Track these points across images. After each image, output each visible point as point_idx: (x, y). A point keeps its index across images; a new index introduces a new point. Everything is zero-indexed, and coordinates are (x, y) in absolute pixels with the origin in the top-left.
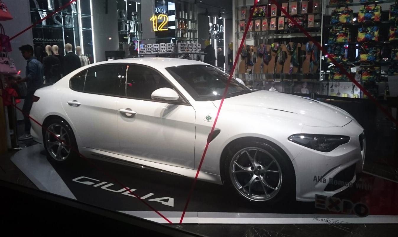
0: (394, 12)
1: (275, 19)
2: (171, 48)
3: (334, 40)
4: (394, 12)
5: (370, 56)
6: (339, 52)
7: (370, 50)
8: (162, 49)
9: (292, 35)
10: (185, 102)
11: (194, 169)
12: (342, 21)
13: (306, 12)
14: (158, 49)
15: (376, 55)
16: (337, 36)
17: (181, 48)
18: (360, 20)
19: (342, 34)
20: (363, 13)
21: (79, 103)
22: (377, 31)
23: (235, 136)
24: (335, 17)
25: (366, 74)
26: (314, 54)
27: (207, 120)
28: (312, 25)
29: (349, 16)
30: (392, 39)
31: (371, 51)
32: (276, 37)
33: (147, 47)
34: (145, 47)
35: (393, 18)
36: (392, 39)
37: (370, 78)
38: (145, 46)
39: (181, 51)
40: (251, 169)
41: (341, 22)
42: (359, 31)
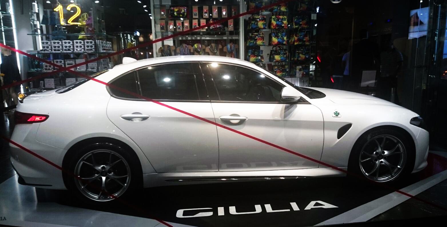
0: (297, 22)
1: (197, 20)
2: (92, 46)
3: (255, 42)
4: (297, 22)
5: (282, 56)
6: (258, 53)
7: (281, 52)
8: (77, 47)
9: (210, 37)
10: (302, 101)
11: (318, 168)
12: (260, 26)
13: (226, 17)
14: (70, 47)
15: (286, 56)
16: (257, 39)
17: (102, 46)
18: (274, 27)
19: (260, 38)
20: (275, 21)
21: (144, 115)
22: (285, 36)
23: (367, 128)
24: (255, 23)
25: (279, 72)
26: (234, 54)
27: (336, 116)
28: (232, 28)
29: (265, 22)
30: (297, 43)
31: (282, 53)
32: (182, 38)
33: (53, 44)
34: (49, 44)
35: (297, 26)
36: (297, 43)
37: (283, 74)
38: (49, 42)
39: (102, 50)
40: (384, 153)
41: (259, 27)
42: (272, 36)
